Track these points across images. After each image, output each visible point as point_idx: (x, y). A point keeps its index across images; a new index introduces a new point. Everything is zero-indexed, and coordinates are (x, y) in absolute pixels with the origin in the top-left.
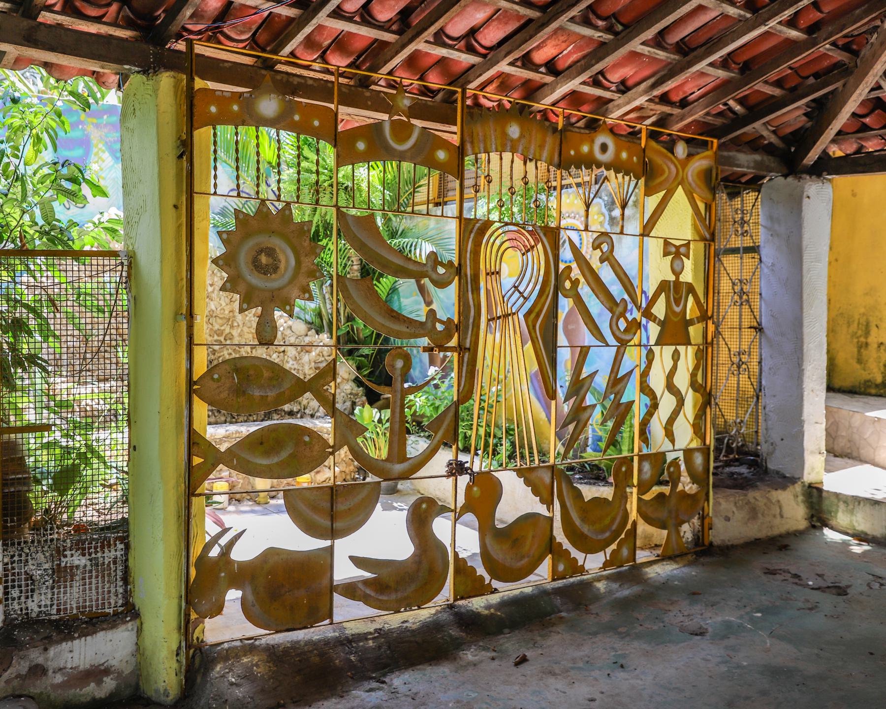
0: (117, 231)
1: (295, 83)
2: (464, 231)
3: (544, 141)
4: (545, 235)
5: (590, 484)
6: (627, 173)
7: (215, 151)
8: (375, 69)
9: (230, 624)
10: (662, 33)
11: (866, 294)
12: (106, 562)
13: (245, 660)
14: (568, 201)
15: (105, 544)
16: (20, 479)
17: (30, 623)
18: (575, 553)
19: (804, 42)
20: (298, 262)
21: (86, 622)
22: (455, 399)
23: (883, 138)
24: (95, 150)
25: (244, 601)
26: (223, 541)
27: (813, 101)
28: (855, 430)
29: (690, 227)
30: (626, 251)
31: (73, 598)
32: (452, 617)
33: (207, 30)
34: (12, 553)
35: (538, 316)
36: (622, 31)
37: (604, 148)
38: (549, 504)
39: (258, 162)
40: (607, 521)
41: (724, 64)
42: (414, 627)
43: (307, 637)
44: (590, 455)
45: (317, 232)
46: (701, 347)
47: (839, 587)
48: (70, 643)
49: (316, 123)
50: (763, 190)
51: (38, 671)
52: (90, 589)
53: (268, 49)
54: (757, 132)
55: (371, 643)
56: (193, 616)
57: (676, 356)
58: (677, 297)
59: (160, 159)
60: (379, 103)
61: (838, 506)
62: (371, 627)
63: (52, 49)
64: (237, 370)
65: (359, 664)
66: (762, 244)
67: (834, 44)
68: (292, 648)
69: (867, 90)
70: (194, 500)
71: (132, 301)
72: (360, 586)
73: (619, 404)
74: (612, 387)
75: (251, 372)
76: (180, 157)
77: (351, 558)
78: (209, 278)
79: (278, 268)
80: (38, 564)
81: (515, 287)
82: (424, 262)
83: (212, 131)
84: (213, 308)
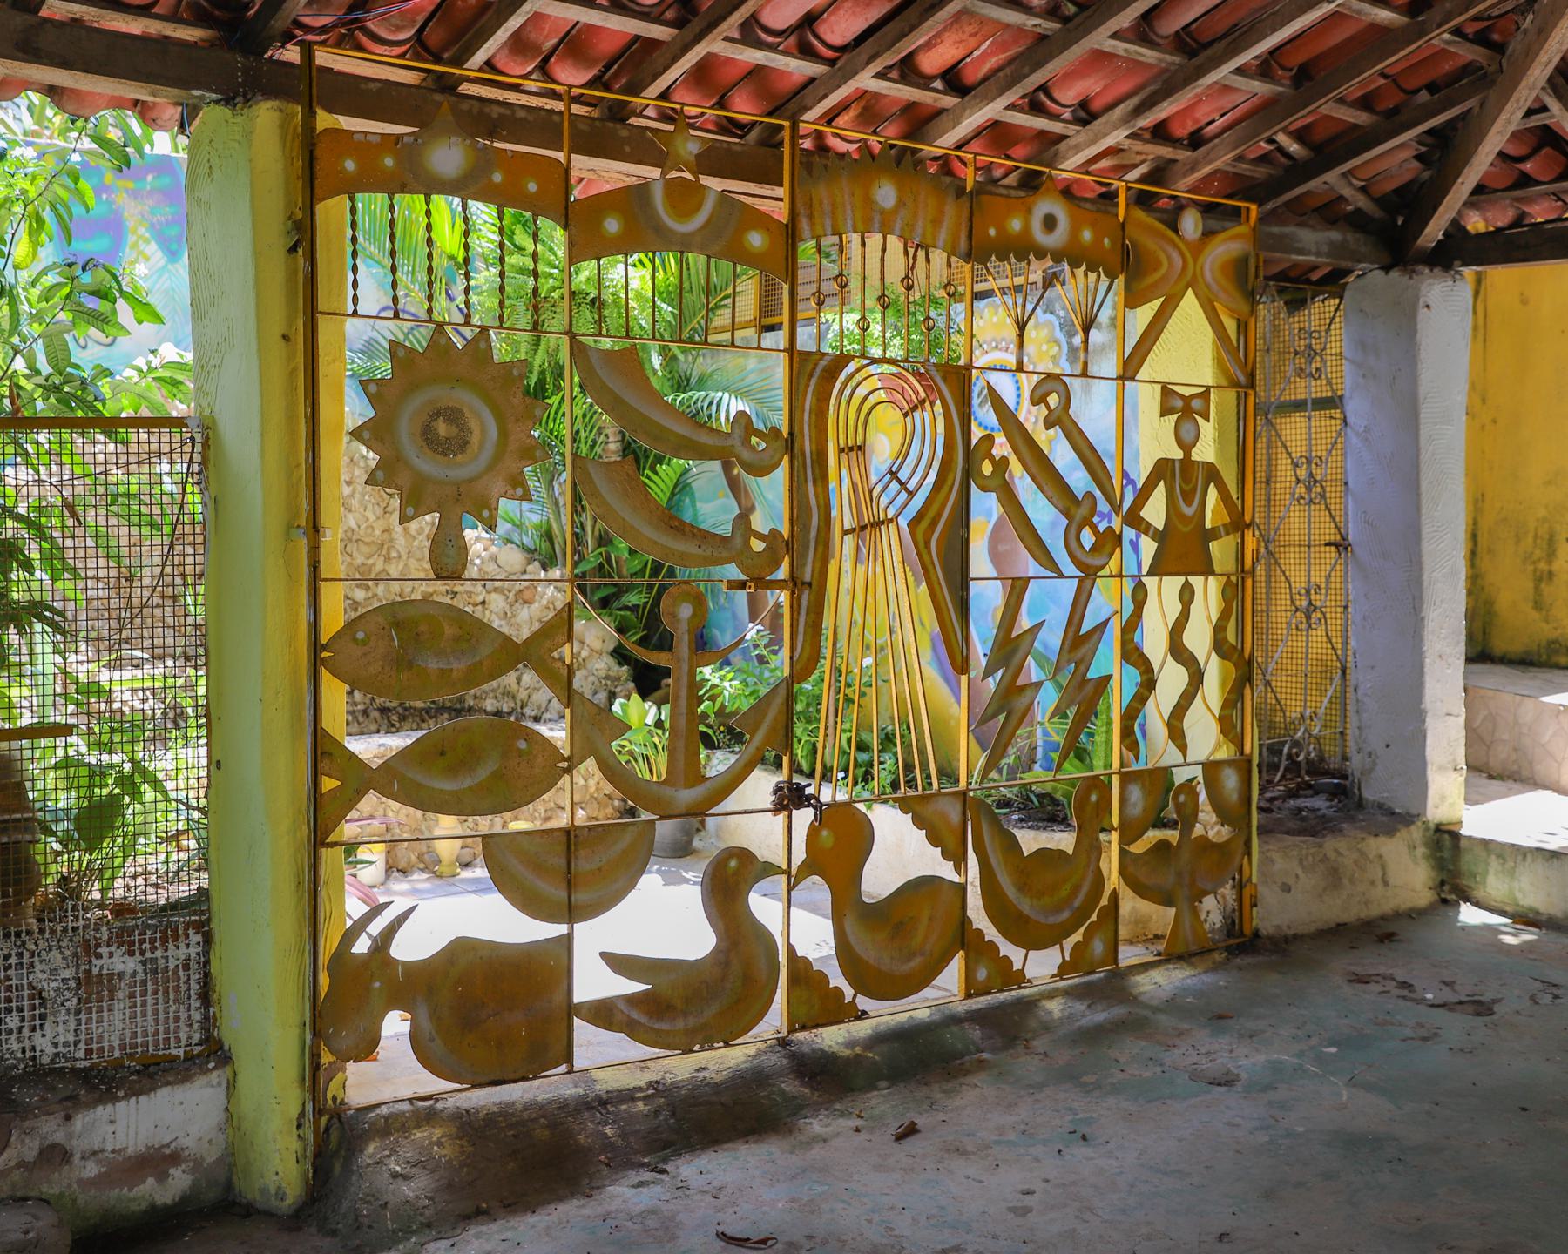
0: (181, 383)
1: (495, 115)
2: (799, 374)
3: (942, 212)
4: (945, 379)
5: (1038, 828)
6: (1091, 268)
7: (354, 239)
8: (635, 89)
9: (392, 1069)
10: (1148, 16)
11: (1549, 483)
12: (172, 966)
13: (419, 1135)
14: (995, 319)
15: (170, 935)
16: (18, 820)
17: (39, 1074)
18: (1007, 949)
19: (1404, 28)
20: (504, 434)
21: (138, 1072)
22: (787, 672)
23: (1559, 199)
24: (131, 239)
25: (416, 1039)
26: (376, 927)
27: (1430, 132)
28: (1525, 730)
29: (1210, 362)
30: (1094, 409)
31: (114, 1028)
32: (785, 1062)
33: (335, 26)
34: (6, 952)
35: (934, 524)
36: (1076, 15)
37: (1050, 223)
38: (959, 862)
39: (430, 256)
40: (1065, 891)
41: (1264, 68)
42: (718, 1078)
43: (527, 1097)
44: (1038, 775)
45: (541, 383)
46: (1233, 579)
47: (1479, 1003)
48: (109, 1107)
49: (532, 187)
50: (1347, 294)
51: (56, 1155)
52: (144, 1014)
53: (446, 56)
54: (1332, 189)
55: (640, 1106)
56: (326, 1058)
57: (1187, 595)
58: (1187, 488)
59: (257, 254)
60: (644, 149)
61: (1488, 864)
62: (640, 1079)
63: (65, 64)
64: (398, 625)
65: (620, 1142)
66: (1347, 394)
67: (1457, 32)
68: (500, 1114)
69: (1520, 114)
70: (325, 853)
71: (211, 505)
72: (622, 1006)
73: (1084, 682)
74: (1070, 652)
75: (423, 628)
76: (293, 249)
77: (604, 955)
78: (348, 462)
79: (468, 442)
80: (52, 970)
81: (891, 472)
82: (725, 428)
83: (348, 204)
84: (353, 524)
